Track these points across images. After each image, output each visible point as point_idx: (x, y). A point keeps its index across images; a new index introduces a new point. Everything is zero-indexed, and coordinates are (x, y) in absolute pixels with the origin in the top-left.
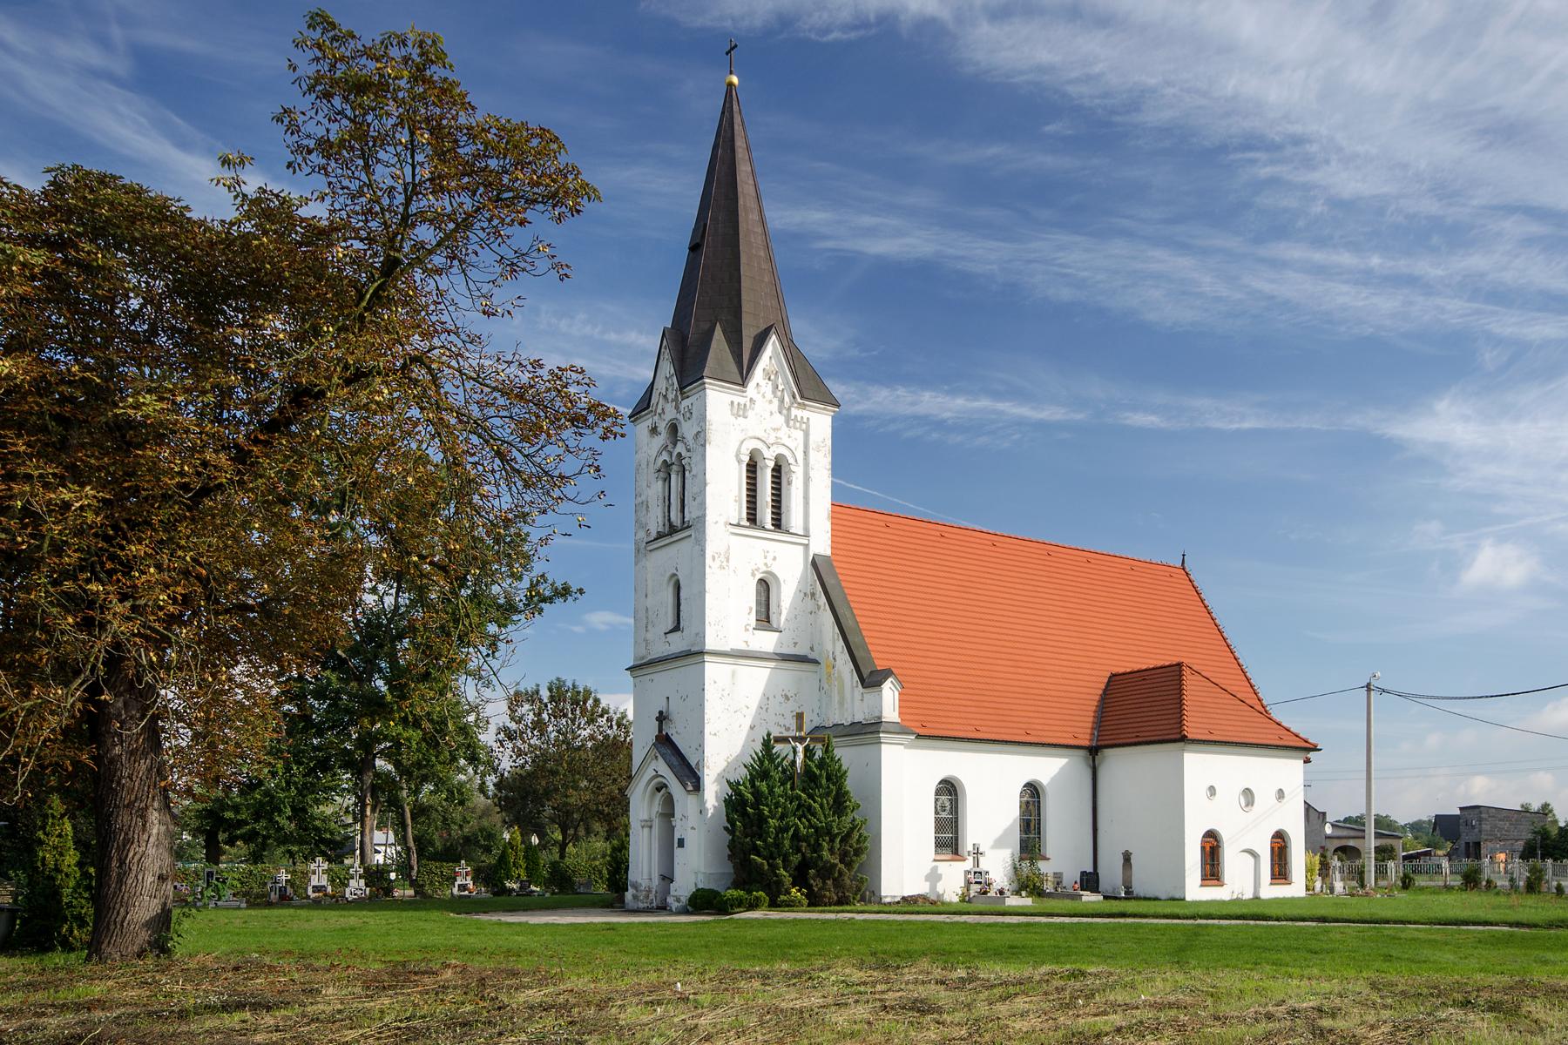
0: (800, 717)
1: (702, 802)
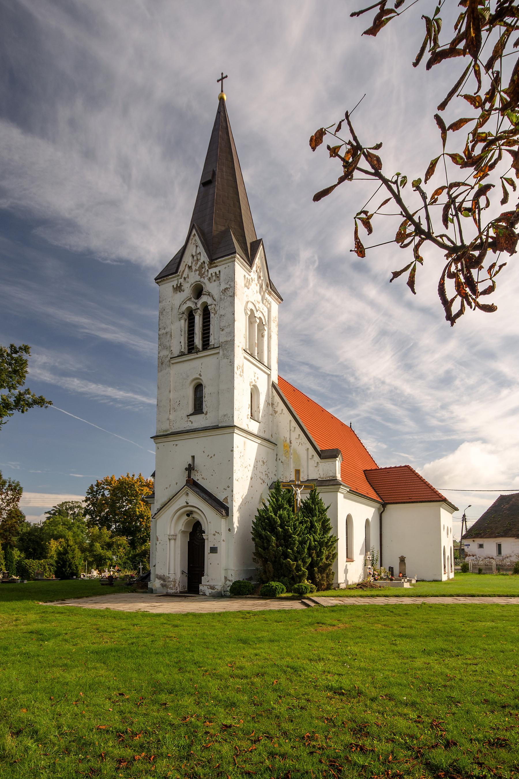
0: (298, 472)
1: (232, 523)
